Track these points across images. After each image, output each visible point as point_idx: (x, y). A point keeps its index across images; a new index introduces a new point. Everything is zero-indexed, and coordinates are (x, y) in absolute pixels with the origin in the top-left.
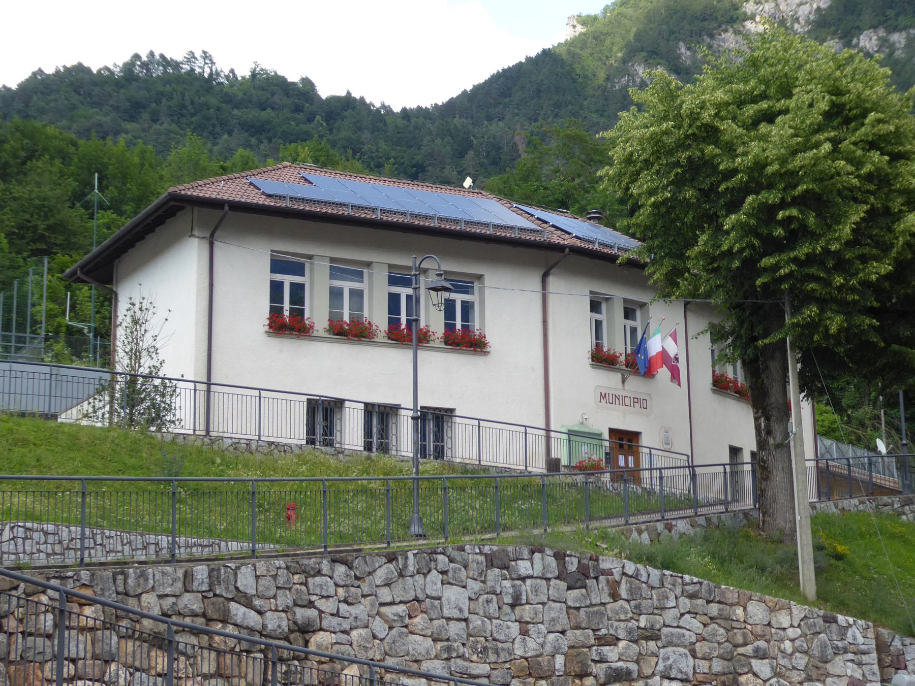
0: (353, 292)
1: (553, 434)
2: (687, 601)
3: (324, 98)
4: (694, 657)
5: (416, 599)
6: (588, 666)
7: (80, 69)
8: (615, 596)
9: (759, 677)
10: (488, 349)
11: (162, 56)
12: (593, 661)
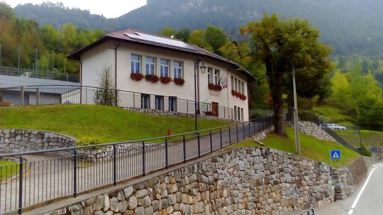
2: (289, 160)
3: (14, 8)
4: (292, 176)
5: (235, 166)
6: (269, 181)
7: (30, 4)
8: (274, 160)
9: (306, 181)
11: (51, 2)
12: (271, 179)
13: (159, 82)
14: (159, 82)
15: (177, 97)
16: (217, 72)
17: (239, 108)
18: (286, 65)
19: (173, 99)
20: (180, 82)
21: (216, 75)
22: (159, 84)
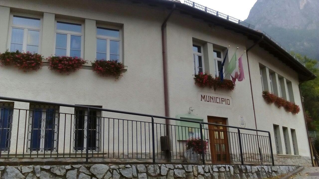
0: (73, 37)
1: (172, 122)
10: (125, 68)
13: (45, 69)
14: (45, 69)
15: (101, 107)
16: (220, 51)
17: (285, 129)
19: (88, 117)
20: (110, 69)
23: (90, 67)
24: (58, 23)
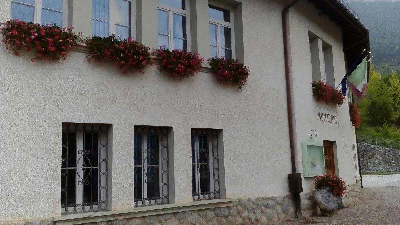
13: (152, 71)
14: (152, 71)
18: (397, 47)
20: (230, 73)
21: (227, 24)
22: (151, 82)
23: (206, 69)
24: (210, 9)
